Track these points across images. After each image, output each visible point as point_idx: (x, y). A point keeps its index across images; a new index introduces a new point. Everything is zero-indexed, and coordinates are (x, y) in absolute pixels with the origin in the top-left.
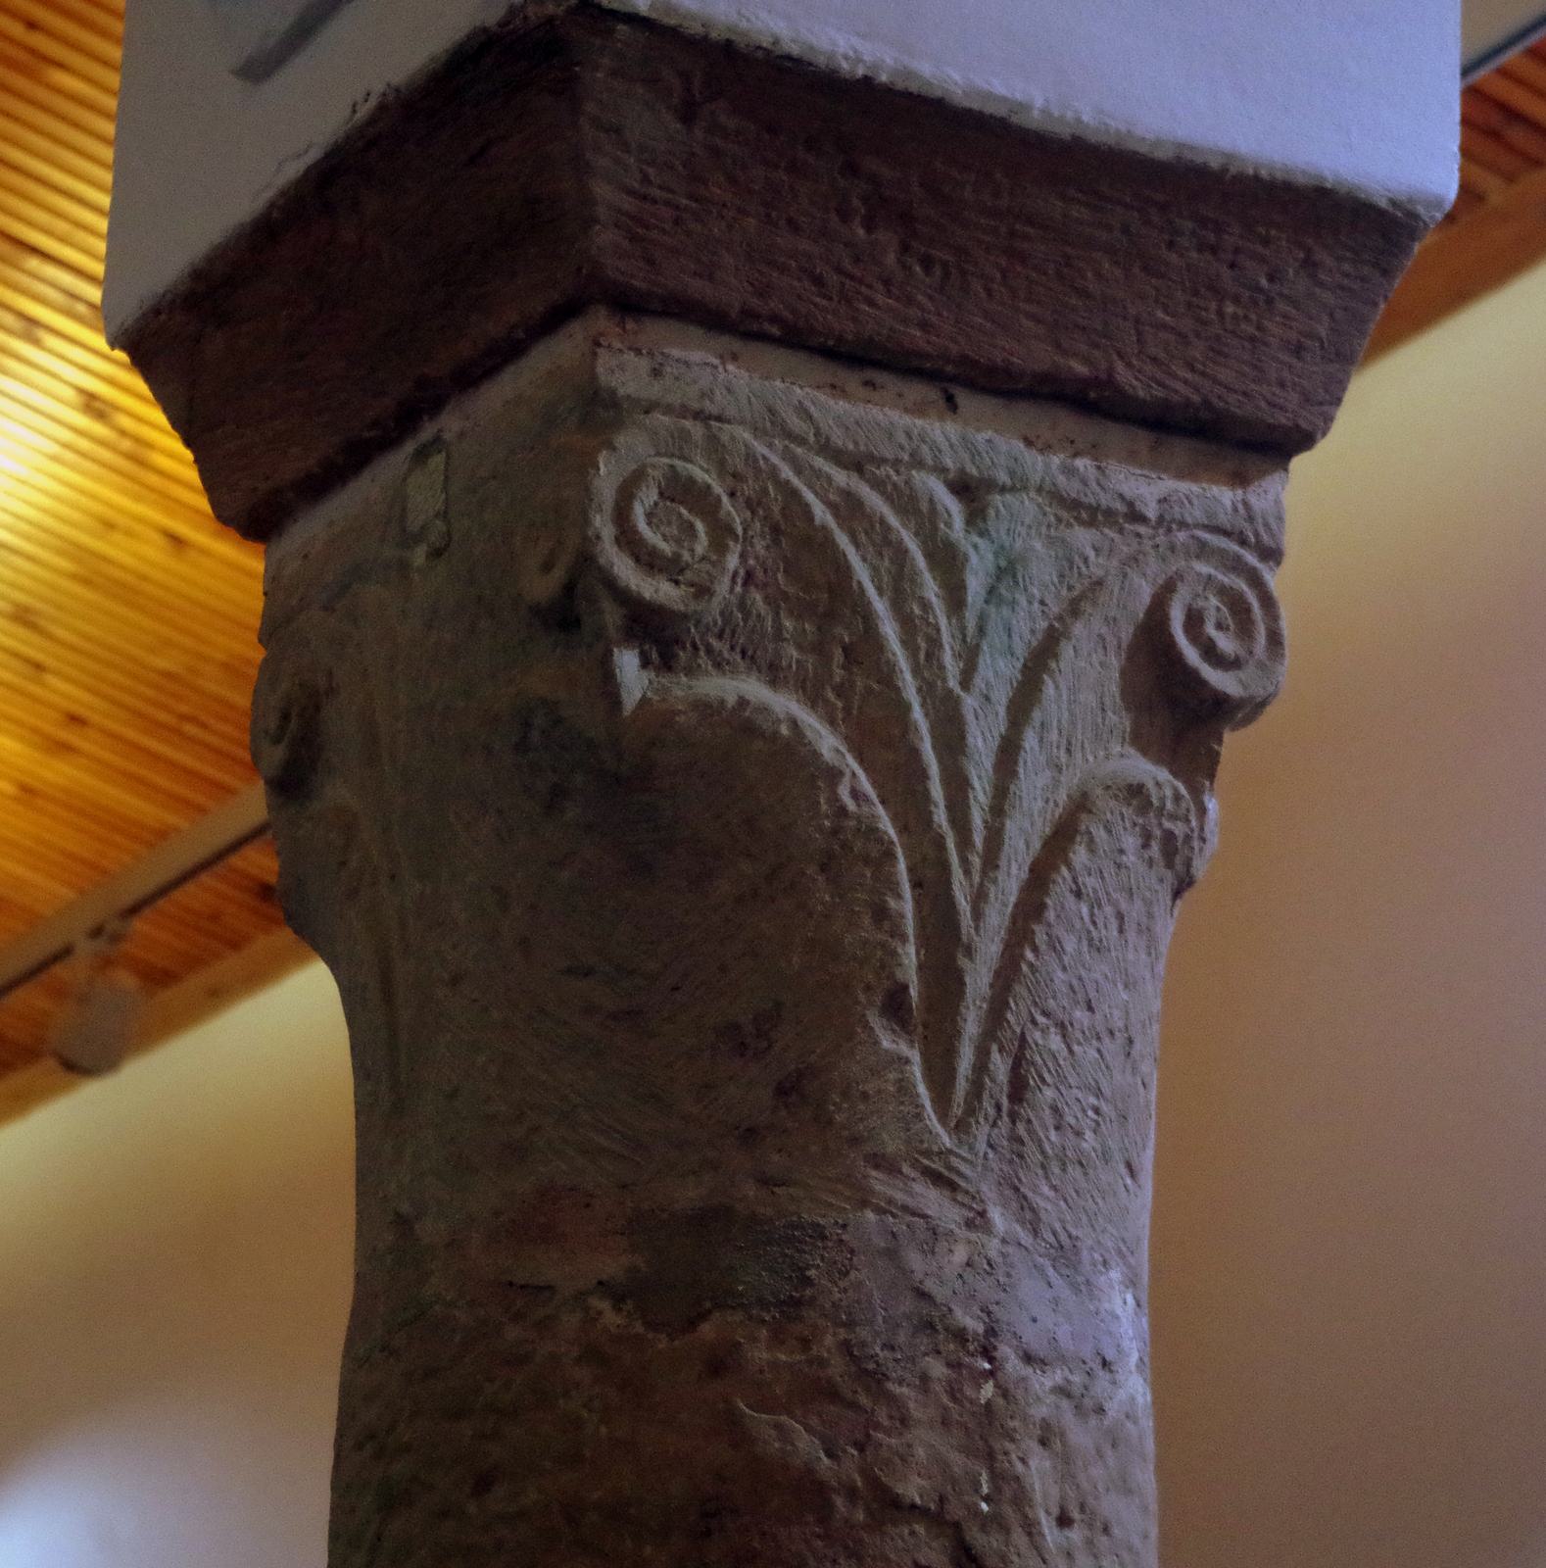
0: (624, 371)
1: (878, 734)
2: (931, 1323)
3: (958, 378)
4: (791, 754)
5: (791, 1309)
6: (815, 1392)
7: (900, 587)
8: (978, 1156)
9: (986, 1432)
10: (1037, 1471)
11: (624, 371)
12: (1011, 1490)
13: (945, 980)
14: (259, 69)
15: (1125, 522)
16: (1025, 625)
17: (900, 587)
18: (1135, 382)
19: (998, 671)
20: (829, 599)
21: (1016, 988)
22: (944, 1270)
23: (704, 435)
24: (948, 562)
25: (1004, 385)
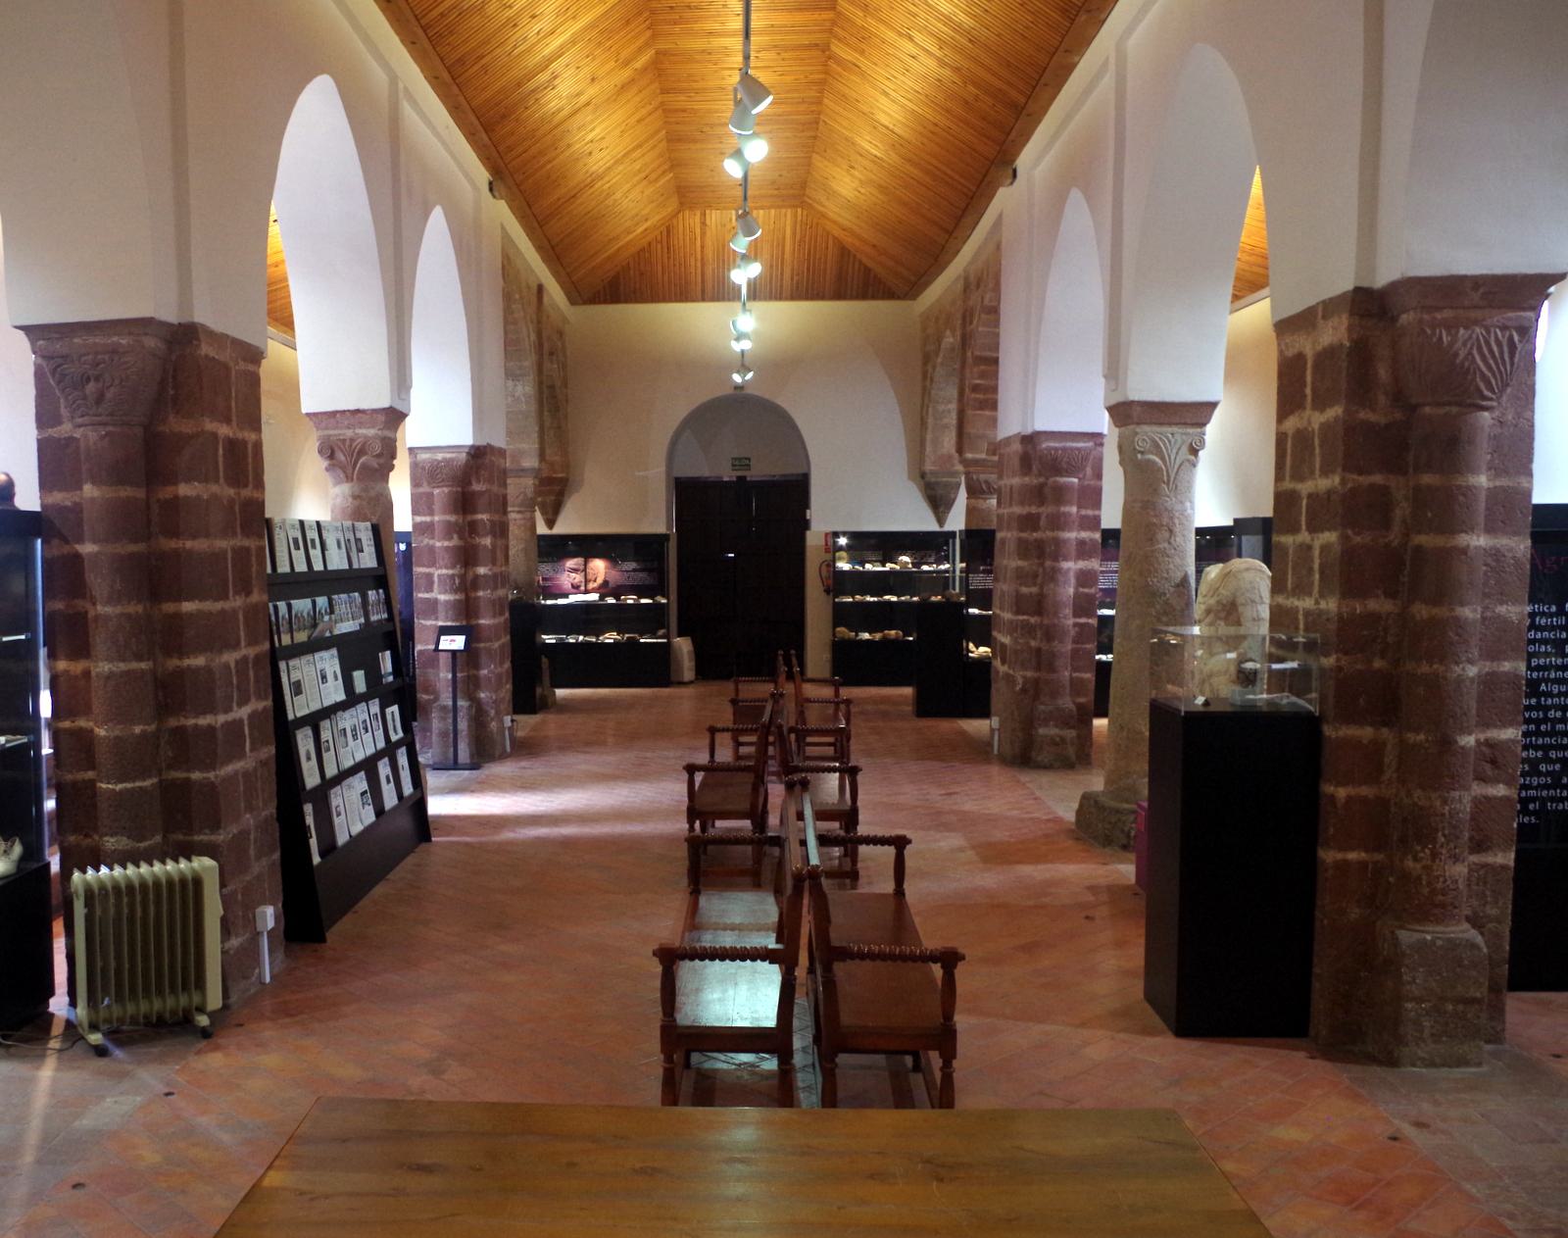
0: (1138, 430)
1: (1163, 459)
2: (1166, 509)
3: (1170, 424)
4: (1154, 463)
5: (1154, 509)
6: (1156, 516)
7: (1165, 444)
8: (1172, 495)
9: (1172, 518)
10: (1177, 521)
11: (1138, 430)
12: (1174, 524)
13: (1169, 481)
14: (1000, 216)
15: (598, 636)
16: (1177, 446)
17: (1165, 444)
18: (1188, 421)
19: (1174, 451)
20: (1158, 446)
21: (553, 105)
22: (1168, 505)
23: (1056, 614)
24: (1170, 442)
25: (1176, 424)
